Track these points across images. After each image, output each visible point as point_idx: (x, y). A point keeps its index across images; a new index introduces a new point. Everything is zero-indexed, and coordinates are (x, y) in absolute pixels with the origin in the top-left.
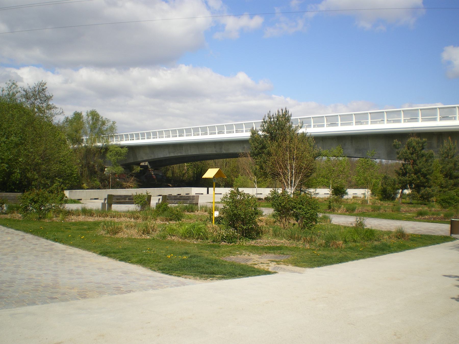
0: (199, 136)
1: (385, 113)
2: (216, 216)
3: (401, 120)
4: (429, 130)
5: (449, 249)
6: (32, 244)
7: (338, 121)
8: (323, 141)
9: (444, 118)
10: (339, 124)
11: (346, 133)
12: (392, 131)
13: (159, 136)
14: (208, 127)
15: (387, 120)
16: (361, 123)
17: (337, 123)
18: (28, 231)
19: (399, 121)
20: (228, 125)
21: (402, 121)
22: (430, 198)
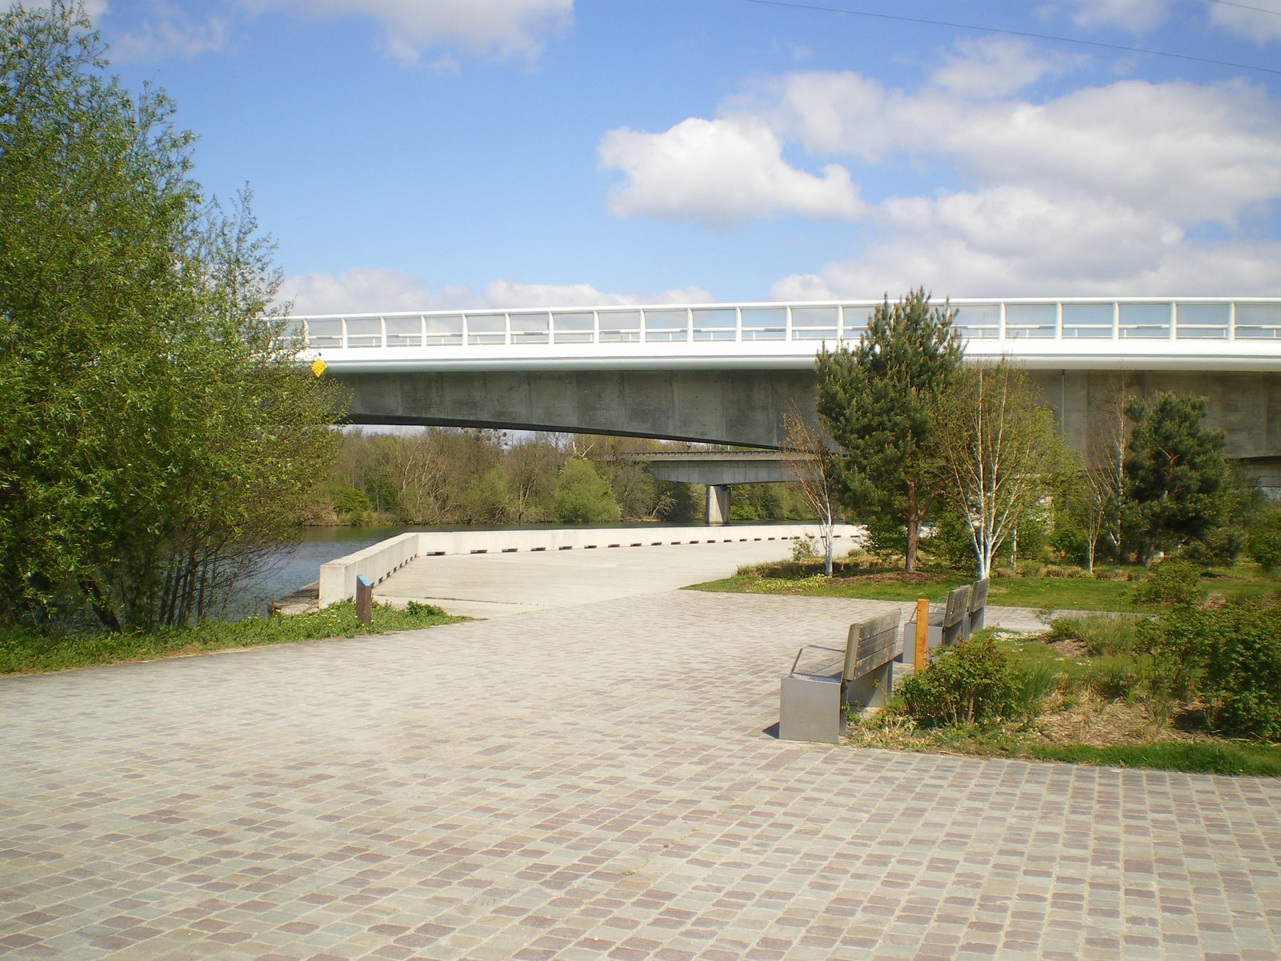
1: (739, 311)
2: (922, 535)
4: (1207, 364)
8: (529, 384)
9: (394, 340)
11: (354, 367)
12: (591, 364)
18: (134, 571)
19: (730, 336)
21: (739, 335)
22: (1169, 493)
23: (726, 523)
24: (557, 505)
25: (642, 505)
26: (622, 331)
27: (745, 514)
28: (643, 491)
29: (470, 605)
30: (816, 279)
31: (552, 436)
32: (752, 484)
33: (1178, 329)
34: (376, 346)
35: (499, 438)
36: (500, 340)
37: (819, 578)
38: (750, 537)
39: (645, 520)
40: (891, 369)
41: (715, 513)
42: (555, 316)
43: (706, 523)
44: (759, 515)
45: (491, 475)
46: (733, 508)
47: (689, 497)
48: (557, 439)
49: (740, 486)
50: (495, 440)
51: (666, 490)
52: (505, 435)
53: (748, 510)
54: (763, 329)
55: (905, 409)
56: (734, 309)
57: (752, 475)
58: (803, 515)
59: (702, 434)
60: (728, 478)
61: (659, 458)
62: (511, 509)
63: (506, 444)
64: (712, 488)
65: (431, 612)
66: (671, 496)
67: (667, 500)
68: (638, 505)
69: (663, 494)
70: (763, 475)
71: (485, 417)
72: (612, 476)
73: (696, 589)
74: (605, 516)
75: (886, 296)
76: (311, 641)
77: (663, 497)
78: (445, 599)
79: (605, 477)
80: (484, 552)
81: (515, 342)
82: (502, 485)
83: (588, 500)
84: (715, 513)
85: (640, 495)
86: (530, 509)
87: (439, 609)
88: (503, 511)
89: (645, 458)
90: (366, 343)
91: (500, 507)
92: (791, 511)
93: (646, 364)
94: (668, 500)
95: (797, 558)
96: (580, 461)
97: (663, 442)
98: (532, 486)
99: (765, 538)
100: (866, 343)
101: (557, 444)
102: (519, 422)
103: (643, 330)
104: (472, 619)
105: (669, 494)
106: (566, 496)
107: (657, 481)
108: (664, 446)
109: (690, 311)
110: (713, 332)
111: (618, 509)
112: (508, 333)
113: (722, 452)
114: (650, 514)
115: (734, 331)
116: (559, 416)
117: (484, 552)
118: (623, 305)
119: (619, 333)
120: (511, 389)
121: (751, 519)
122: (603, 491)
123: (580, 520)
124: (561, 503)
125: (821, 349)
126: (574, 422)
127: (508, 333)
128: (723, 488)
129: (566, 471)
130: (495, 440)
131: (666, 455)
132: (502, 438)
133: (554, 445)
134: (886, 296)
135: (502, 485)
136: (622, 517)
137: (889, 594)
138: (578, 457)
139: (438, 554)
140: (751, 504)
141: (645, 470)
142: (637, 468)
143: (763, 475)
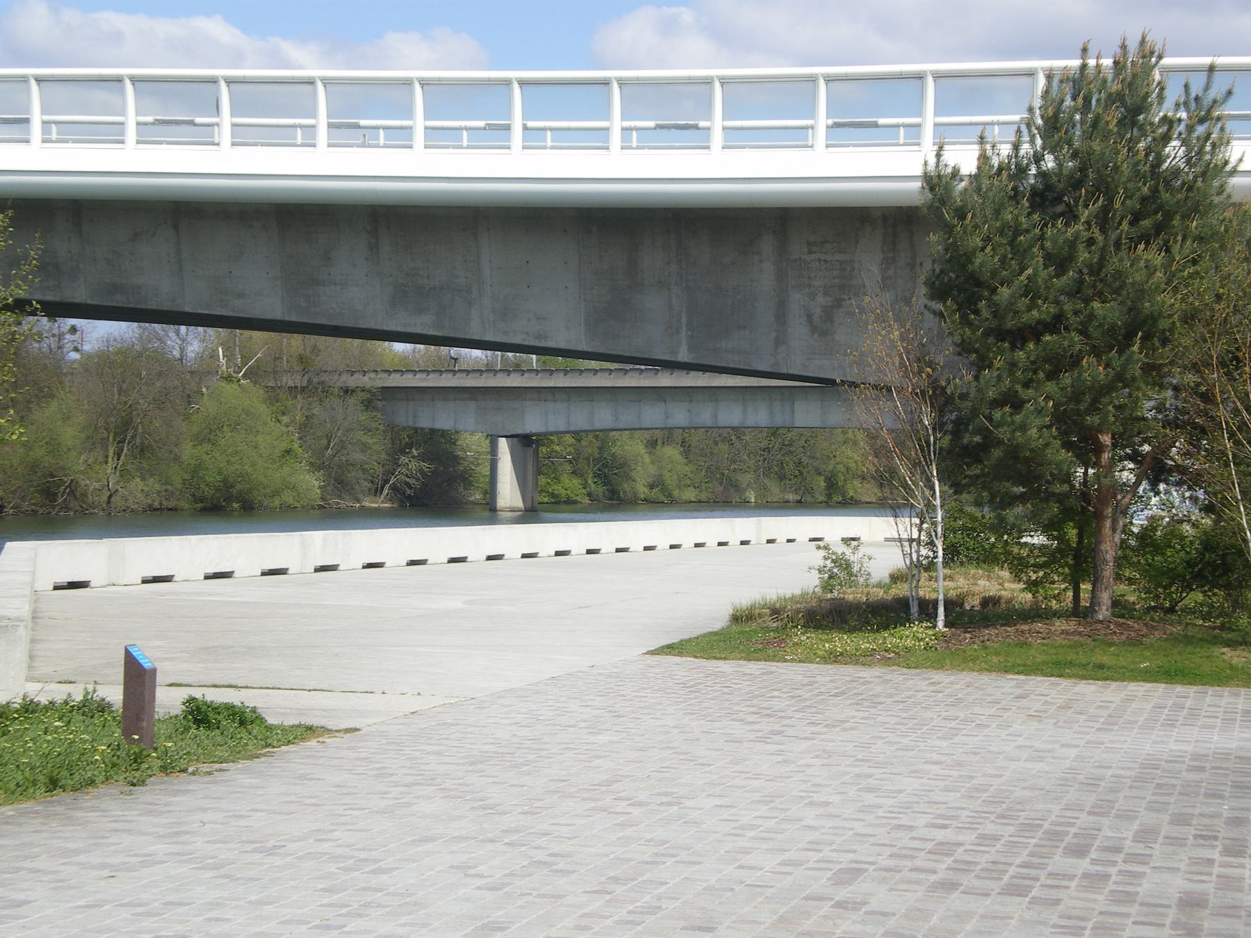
0: (808, 152)
3: (411, 128)
5: (1056, 933)
6: (412, 796)
7: (708, 113)
8: (176, 227)
10: (717, 137)
12: (457, 193)
13: (530, 124)
14: (717, 85)
15: (525, 128)
16: (361, 132)
17: (702, 124)
19: (599, 139)
20: (439, 82)
21: (616, 137)
23: (530, 514)
24: (187, 476)
25: (360, 474)
26: (363, 122)
27: (563, 492)
28: (365, 448)
29: (319, 699)
30: (687, 16)
31: (172, 335)
32: (577, 435)
33: (234, 125)
34: (303, 145)
35: (60, 337)
36: (112, 134)
37: (914, 634)
38: (663, 544)
39: (367, 504)
40: (1086, 206)
41: (508, 492)
42: (233, 86)
43: (488, 512)
44: (589, 495)
45: (46, 413)
46: (543, 480)
47: (456, 460)
48: (183, 340)
49: (554, 438)
50: (53, 342)
51: (410, 446)
52: (73, 330)
53: (569, 485)
54: (651, 124)
55: (1117, 285)
56: (606, 83)
57: (580, 417)
58: (676, 493)
59: (539, 337)
60: (534, 421)
61: (395, 381)
62: (90, 484)
63: (76, 350)
64: (503, 444)
65: (310, 728)
66: (422, 458)
67: (412, 466)
68: (353, 475)
69: (404, 453)
70: (603, 416)
71: (80, 294)
72: (299, 417)
73: (680, 654)
74: (288, 497)
75: (1085, 50)
76: (59, 795)
77: (404, 459)
78: (200, 686)
79: (285, 419)
80: (166, 579)
81: (634, 144)
82: (70, 434)
83: (253, 465)
84: (508, 492)
85: (358, 456)
86: (132, 485)
87: (254, 710)
88: (73, 488)
89: (367, 381)
90: (278, 137)
91: (67, 480)
92: (651, 487)
93: (12, 185)
94: (413, 465)
95: (827, 586)
96: (235, 386)
97: (399, 347)
98: (133, 437)
99: (663, 544)
100: (1026, 148)
101: (182, 350)
102: (154, 307)
103: (419, 123)
104: (326, 731)
105: (415, 452)
106: (206, 458)
107: (391, 428)
108: (404, 358)
109: (516, 86)
110: (551, 129)
111: (312, 483)
112: (131, 119)
113: (518, 369)
114: (377, 491)
115: (607, 129)
116: (241, 295)
117: (166, 579)
118: (301, 67)
119: (358, 126)
120: (135, 237)
121: (575, 502)
122: (284, 445)
123: (235, 505)
124: (197, 470)
125: (932, 161)
126: (273, 308)
127: (131, 119)
128: (525, 443)
129: (207, 406)
130: (53, 342)
131: (410, 376)
132: (68, 336)
133: (176, 353)
134: (1085, 50)
135: (70, 434)
136: (323, 499)
137: (1084, 666)
138: (228, 379)
139: (73, 585)
140: (574, 473)
141: (368, 405)
142: (351, 401)
143: (603, 416)
